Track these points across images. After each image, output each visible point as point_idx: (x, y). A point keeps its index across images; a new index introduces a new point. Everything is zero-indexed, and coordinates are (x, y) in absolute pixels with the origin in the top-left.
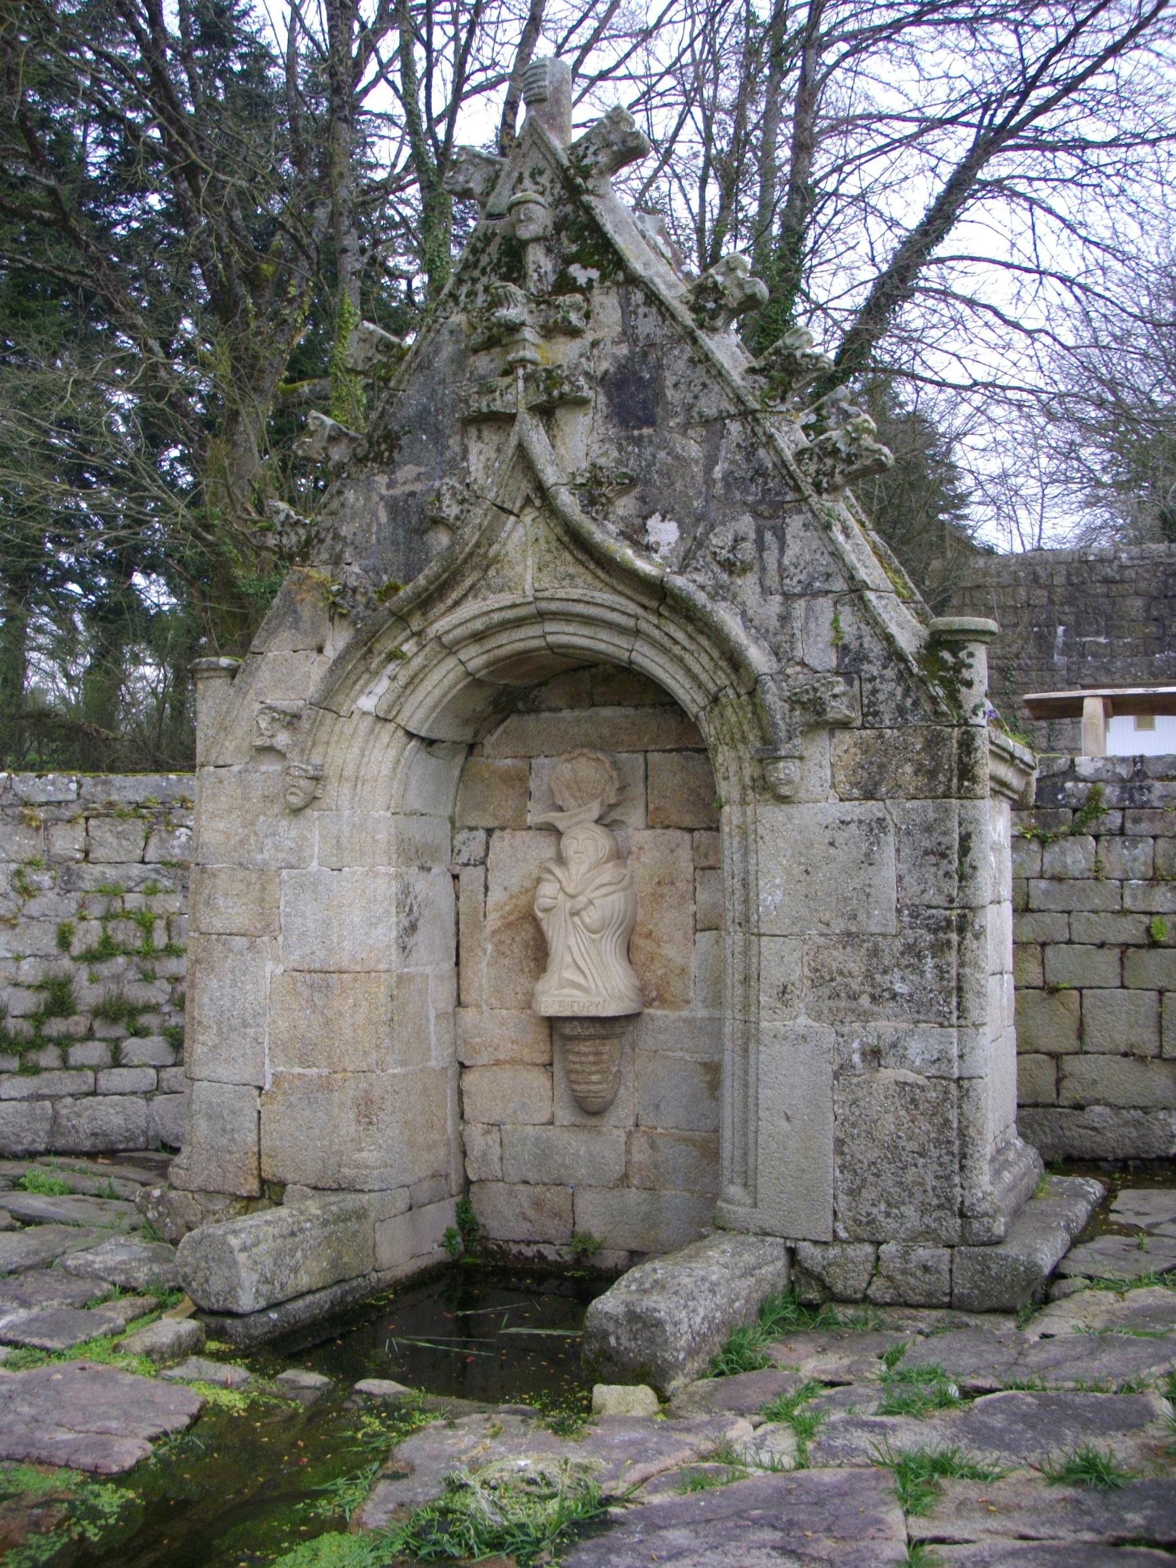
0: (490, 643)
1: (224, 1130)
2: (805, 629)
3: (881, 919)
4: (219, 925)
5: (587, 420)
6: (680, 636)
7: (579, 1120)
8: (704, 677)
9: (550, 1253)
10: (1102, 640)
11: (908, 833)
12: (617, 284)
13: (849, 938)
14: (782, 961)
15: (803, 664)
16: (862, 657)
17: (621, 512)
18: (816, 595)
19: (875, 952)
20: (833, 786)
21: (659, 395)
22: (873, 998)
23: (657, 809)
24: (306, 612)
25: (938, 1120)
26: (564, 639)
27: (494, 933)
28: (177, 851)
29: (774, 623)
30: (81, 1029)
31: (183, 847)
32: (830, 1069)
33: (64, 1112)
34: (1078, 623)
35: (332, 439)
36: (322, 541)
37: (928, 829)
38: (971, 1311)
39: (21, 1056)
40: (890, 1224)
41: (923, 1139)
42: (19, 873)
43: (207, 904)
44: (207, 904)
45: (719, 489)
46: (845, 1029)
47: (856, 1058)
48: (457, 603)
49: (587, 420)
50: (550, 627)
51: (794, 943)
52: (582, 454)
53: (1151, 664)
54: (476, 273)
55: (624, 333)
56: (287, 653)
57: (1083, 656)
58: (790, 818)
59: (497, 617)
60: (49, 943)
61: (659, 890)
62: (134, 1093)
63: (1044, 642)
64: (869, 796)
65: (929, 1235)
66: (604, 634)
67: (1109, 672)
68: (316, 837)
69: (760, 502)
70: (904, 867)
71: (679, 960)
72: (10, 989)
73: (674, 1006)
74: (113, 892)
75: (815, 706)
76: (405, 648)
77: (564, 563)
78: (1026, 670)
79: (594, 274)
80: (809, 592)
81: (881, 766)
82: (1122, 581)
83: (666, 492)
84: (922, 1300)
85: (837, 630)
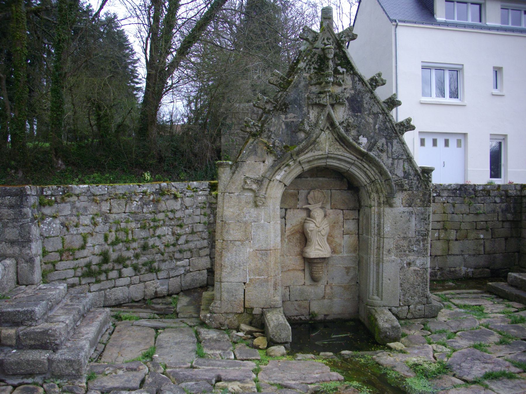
1: (233, 295)
2: (397, 167)
3: (411, 234)
4: (231, 238)
5: (343, 109)
6: (367, 166)
7: (312, 283)
8: (371, 176)
9: (303, 318)
11: (418, 215)
12: (351, 74)
13: (404, 238)
14: (389, 244)
15: (396, 175)
17: (352, 134)
18: (399, 159)
19: (410, 241)
20: (402, 204)
22: (409, 251)
24: (259, 151)
25: (422, 277)
26: (332, 164)
27: (288, 236)
28: (133, 209)
29: (390, 165)
30: (111, 267)
31: (135, 207)
32: (399, 268)
33: (108, 294)
35: (266, 102)
36: (265, 131)
37: (422, 214)
38: (428, 318)
39: (96, 277)
40: (412, 301)
41: (419, 282)
42: (93, 218)
43: (227, 232)
44: (227, 232)
45: (377, 131)
47: (405, 265)
48: (307, 153)
49: (343, 109)
50: (328, 160)
51: (392, 239)
52: (342, 117)
54: (311, 63)
55: (353, 87)
56: (253, 162)
58: (392, 211)
59: (316, 157)
60: (102, 240)
62: (125, 285)
64: (410, 206)
65: (420, 303)
66: (343, 163)
68: (263, 213)
69: (387, 135)
71: (339, 242)
72: (92, 256)
73: (338, 253)
74: (117, 223)
75: (402, 186)
76: (290, 163)
77: (337, 145)
79: (345, 70)
80: (398, 158)
81: (413, 199)
83: (364, 130)
85: (404, 168)
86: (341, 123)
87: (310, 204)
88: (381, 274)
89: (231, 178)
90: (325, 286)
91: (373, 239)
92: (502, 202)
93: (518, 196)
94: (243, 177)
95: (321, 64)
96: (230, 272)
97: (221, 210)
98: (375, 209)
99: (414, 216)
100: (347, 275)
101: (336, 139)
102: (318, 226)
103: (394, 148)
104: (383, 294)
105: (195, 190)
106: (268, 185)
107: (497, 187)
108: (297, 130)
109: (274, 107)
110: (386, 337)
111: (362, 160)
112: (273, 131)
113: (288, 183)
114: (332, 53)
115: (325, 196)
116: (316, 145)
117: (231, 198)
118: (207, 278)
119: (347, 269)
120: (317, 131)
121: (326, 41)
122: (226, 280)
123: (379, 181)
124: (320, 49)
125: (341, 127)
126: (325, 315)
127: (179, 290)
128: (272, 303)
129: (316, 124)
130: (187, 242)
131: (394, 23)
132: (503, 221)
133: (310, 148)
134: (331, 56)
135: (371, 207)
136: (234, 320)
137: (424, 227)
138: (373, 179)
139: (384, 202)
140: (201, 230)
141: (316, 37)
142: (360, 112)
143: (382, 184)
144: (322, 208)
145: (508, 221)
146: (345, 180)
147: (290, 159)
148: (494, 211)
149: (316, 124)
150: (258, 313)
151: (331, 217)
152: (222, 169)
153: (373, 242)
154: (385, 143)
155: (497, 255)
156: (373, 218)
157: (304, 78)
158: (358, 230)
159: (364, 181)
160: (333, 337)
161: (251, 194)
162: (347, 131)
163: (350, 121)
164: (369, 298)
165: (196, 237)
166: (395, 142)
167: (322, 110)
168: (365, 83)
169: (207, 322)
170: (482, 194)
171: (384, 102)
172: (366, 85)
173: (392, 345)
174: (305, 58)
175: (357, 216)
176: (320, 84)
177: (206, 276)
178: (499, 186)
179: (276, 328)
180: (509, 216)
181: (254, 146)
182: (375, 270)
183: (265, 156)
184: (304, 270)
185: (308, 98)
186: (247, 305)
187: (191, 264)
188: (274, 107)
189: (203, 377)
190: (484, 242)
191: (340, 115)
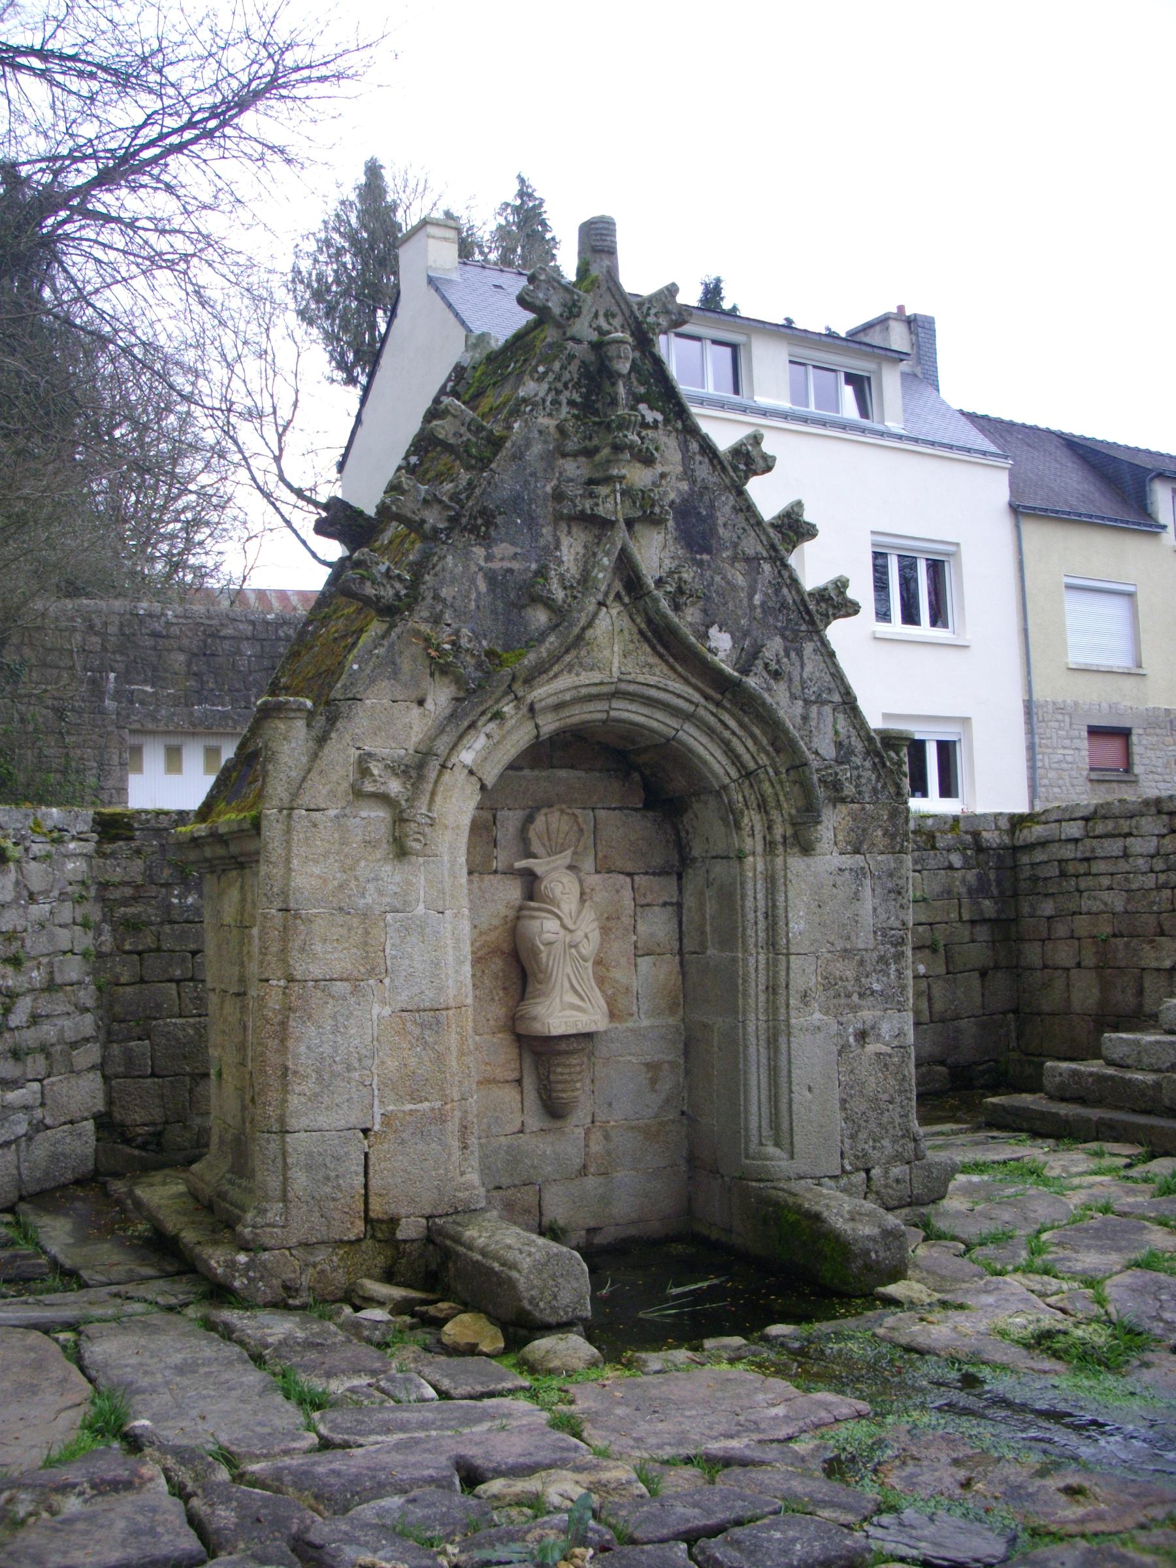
0: (566, 712)
1: (328, 1178)
3: (864, 939)
4: (316, 971)
6: (732, 724)
8: (746, 757)
10: (149, 689)
12: (677, 430)
13: (846, 953)
14: (803, 974)
16: (851, 752)
17: (689, 619)
18: (824, 703)
19: (861, 963)
20: (836, 844)
21: (713, 531)
22: (861, 996)
23: (605, 857)
24: (406, 665)
32: (835, 1049)
34: (127, 671)
36: (424, 599)
38: (923, 1204)
40: (875, 1154)
43: (302, 950)
44: (302, 950)
46: (844, 1019)
47: (851, 1039)
48: (556, 676)
50: (616, 704)
53: (191, 714)
56: (386, 702)
57: (132, 702)
58: (809, 867)
59: (584, 691)
61: (609, 924)
63: (96, 687)
64: (857, 851)
65: (898, 1157)
66: (659, 715)
67: (155, 719)
68: (421, 881)
69: (785, 628)
70: (877, 901)
71: (624, 981)
75: (836, 786)
76: (505, 709)
77: (644, 653)
78: (79, 712)
79: (660, 417)
81: (864, 830)
82: (168, 637)
84: (896, 1203)
85: (836, 733)
86: (660, 582)
87: (535, 856)
88: (784, 1073)
89: (314, 756)
90: (587, 1132)
91: (752, 961)
92: (967, 866)
93: (1006, 848)
94: (354, 754)
95: (589, 393)
96: (316, 1095)
97: (278, 871)
98: (756, 864)
99: (868, 882)
101: (641, 632)
102: (571, 927)
103: (808, 668)
104: (796, 1138)
105: (55, 835)
106: (436, 782)
107: (950, 821)
108: (525, 600)
109: (451, 519)
110: (868, 1267)
111: (718, 704)
112: (449, 599)
113: (490, 780)
114: (627, 358)
115: (581, 830)
116: (583, 653)
118: (96, 1150)
120: (591, 604)
121: (602, 322)
122: (304, 1122)
123: (770, 770)
124: (585, 345)
125: (659, 594)
126: (591, 1231)
127: (13, 1196)
128: (460, 1194)
129: (585, 579)
130: (35, 1019)
132: (973, 922)
133: (568, 658)
134: (624, 367)
135: (741, 857)
136: (335, 1269)
137: (897, 918)
138: (752, 765)
139: (784, 837)
140: (74, 976)
141: (574, 305)
142: (709, 552)
144: (571, 867)
145: (985, 921)
146: (636, 776)
147: (505, 694)
148: (948, 893)
149: (585, 579)
150: (414, 1235)
151: (597, 898)
152: (282, 726)
153: (752, 970)
154: (782, 653)
155: (963, 1023)
156: (750, 893)
157: (540, 432)
158: (681, 940)
159: (721, 771)
160: (675, 1291)
161: (382, 814)
162: (677, 608)
163: (685, 576)
164: (747, 1157)
165: (58, 1004)
166: (808, 648)
167: (599, 538)
168: (720, 462)
169: (237, 1284)
170: (915, 842)
171: (772, 525)
172: (724, 469)
173: (892, 1289)
174: (541, 369)
175: (675, 893)
176: (589, 453)
177: (92, 1140)
178: (956, 819)
179: (540, 1272)
180: (988, 907)
181: (392, 645)
182: (764, 1061)
184: (519, 1081)
185: (558, 496)
186: (377, 1209)
187: (48, 1102)
188: (451, 519)
189: (417, 1474)
190: (929, 987)
191: (654, 553)
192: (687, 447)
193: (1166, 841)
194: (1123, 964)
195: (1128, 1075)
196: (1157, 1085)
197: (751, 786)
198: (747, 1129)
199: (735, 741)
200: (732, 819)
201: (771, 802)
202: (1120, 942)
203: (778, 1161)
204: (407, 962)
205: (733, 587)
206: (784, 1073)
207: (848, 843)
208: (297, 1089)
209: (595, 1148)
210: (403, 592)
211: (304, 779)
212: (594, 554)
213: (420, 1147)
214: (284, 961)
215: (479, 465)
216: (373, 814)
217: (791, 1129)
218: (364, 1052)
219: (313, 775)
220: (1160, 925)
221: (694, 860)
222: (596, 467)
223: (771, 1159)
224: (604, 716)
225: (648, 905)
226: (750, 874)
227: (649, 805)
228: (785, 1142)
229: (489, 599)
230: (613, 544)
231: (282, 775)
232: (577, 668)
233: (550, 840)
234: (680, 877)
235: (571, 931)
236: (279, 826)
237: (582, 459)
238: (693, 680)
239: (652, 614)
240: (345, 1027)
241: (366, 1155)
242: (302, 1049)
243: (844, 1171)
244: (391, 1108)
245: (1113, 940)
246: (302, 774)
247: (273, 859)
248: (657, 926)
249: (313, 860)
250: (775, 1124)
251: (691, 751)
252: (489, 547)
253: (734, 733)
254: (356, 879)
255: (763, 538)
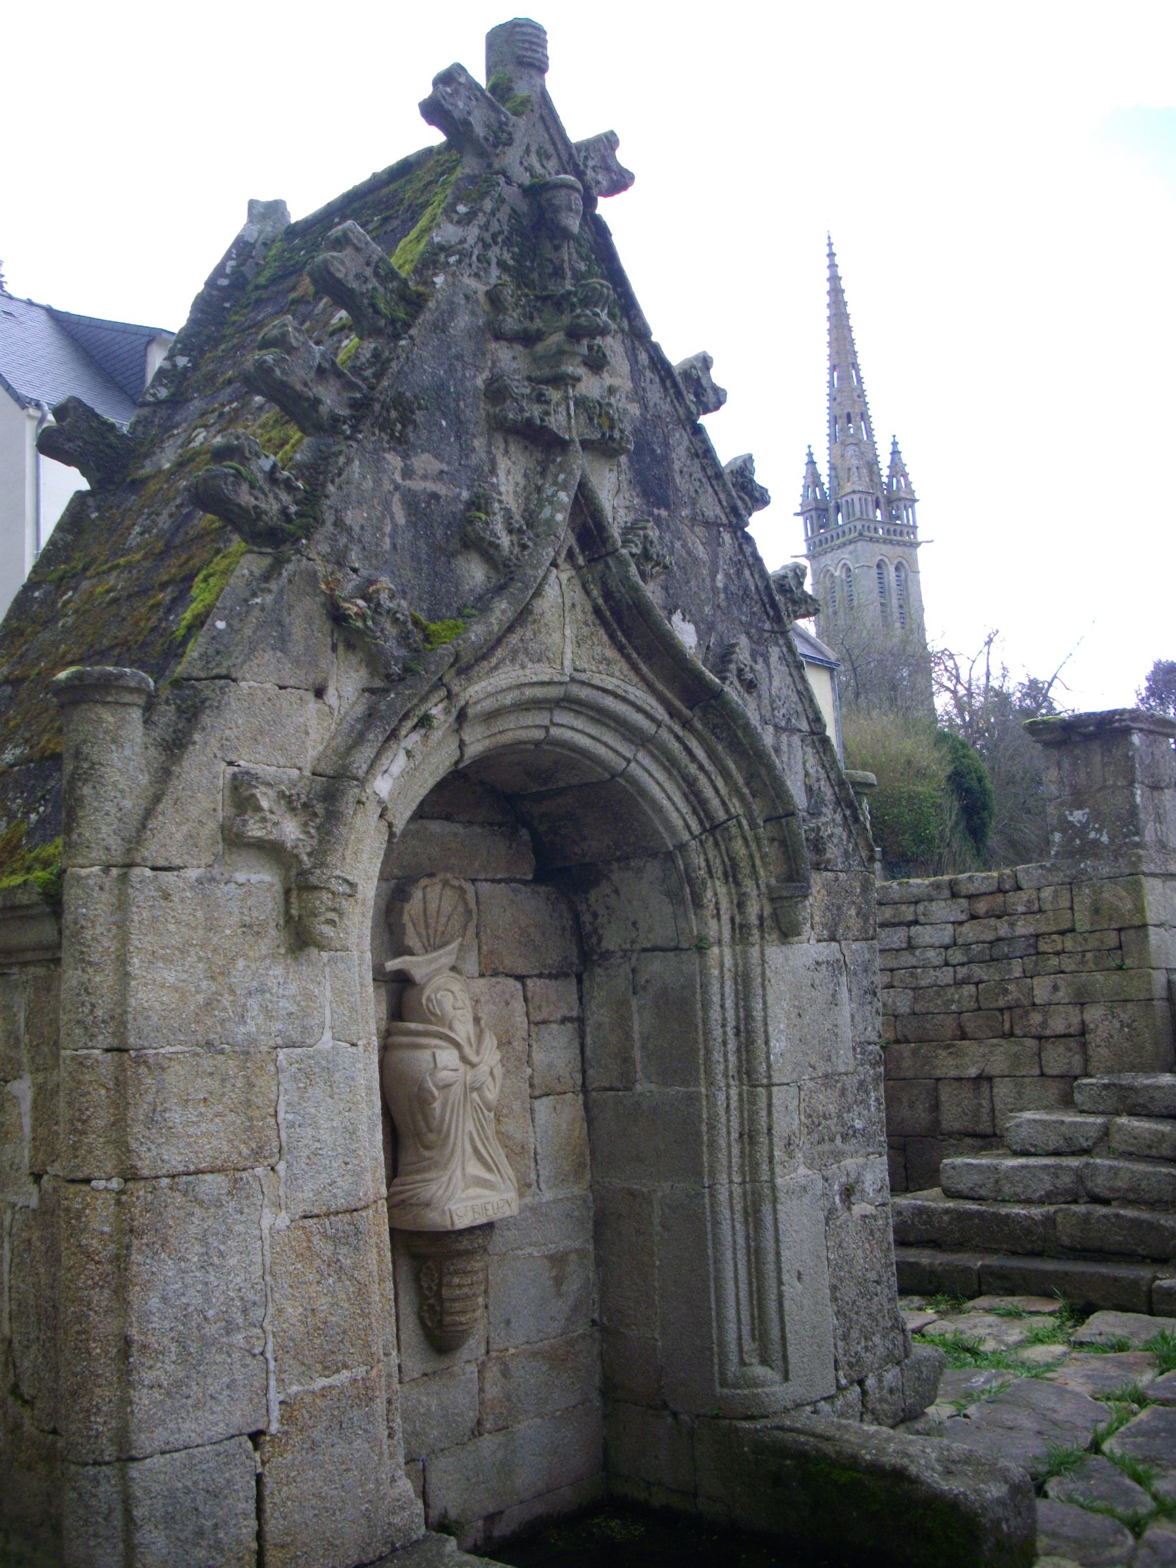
1: (200, 1533)
4: (174, 1158)
6: (700, 753)
8: (715, 803)
14: (786, 1113)
22: (845, 1138)
23: (491, 952)
24: (298, 630)
32: (821, 1216)
40: (868, 1357)
43: (150, 1122)
44: (150, 1122)
46: (828, 1173)
48: (496, 667)
58: (787, 959)
59: (529, 692)
64: (833, 938)
66: (609, 737)
69: (750, 624)
76: (434, 711)
77: (601, 644)
87: (411, 953)
88: (771, 1257)
89: (164, 775)
91: (721, 1097)
96: (179, 1384)
97: (104, 980)
98: (721, 957)
100: (559, 1294)
101: (597, 611)
102: (474, 1059)
108: (455, 544)
111: (686, 724)
116: (529, 634)
117: (166, 897)
119: (557, 1260)
122: (160, 1437)
123: (744, 822)
126: (491, 1518)
131: (32, 411)
135: (701, 948)
138: (721, 815)
139: (761, 918)
142: (667, 507)
143: (757, 839)
146: (524, 834)
152: (109, 717)
153: (722, 1111)
156: (716, 999)
157: (467, 297)
158: (584, 1072)
159: (679, 823)
164: (722, 1386)
168: (675, 385)
176: (528, 339)
182: (741, 1241)
183: (326, 660)
188: (354, 405)
192: (635, 356)
193: (965, 929)
194: (910, 1074)
195: (1004, 1210)
196: (1049, 1220)
197: (716, 844)
198: (722, 1343)
199: (702, 779)
200: (685, 893)
201: (744, 864)
202: (906, 1049)
203: (775, 1390)
204: (310, 1131)
205: (696, 560)
206: (771, 1257)
207: (824, 925)
208: (148, 1376)
209: (492, 1392)
210: (293, 509)
211: (148, 813)
212: (539, 490)
213: (338, 1450)
214: (123, 1147)
215: (389, 330)
216: (254, 878)
217: (783, 1337)
218: (251, 1296)
219: (165, 805)
220: (961, 1027)
221: (606, 955)
222: (536, 360)
223: (756, 1385)
224: (539, 734)
225: (544, 1022)
226: (716, 972)
227: (540, 877)
228: (776, 1356)
229: (409, 535)
230: (571, 473)
231: (108, 806)
232: (521, 656)
233: (427, 927)
234: (580, 981)
235: (473, 1066)
236: (104, 896)
237: (519, 348)
238: (660, 687)
239: (613, 583)
240: (222, 1255)
241: (259, 1478)
242: (154, 1302)
243: (840, 1388)
244: (295, 1388)
245: (896, 1047)
246: (144, 803)
247: (95, 958)
248: (555, 1053)
249: (164, 958)
250: (760, 1333)
251: (643, 792)
252: (405, 456)
253: (701, 767)
254: (232, 991)
255: (722, 496)
